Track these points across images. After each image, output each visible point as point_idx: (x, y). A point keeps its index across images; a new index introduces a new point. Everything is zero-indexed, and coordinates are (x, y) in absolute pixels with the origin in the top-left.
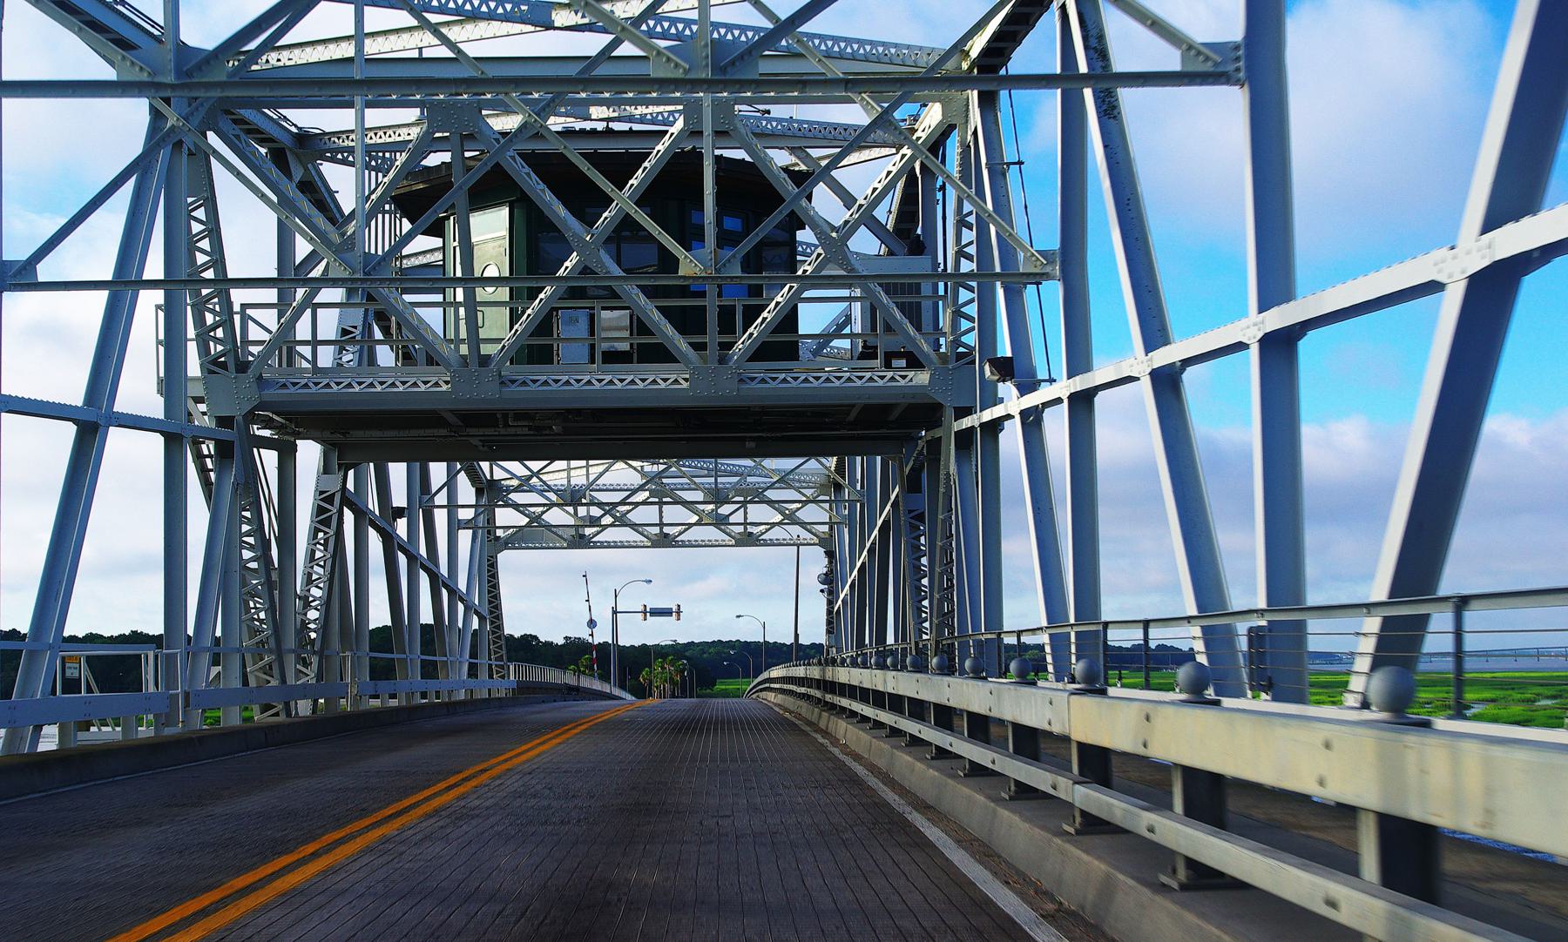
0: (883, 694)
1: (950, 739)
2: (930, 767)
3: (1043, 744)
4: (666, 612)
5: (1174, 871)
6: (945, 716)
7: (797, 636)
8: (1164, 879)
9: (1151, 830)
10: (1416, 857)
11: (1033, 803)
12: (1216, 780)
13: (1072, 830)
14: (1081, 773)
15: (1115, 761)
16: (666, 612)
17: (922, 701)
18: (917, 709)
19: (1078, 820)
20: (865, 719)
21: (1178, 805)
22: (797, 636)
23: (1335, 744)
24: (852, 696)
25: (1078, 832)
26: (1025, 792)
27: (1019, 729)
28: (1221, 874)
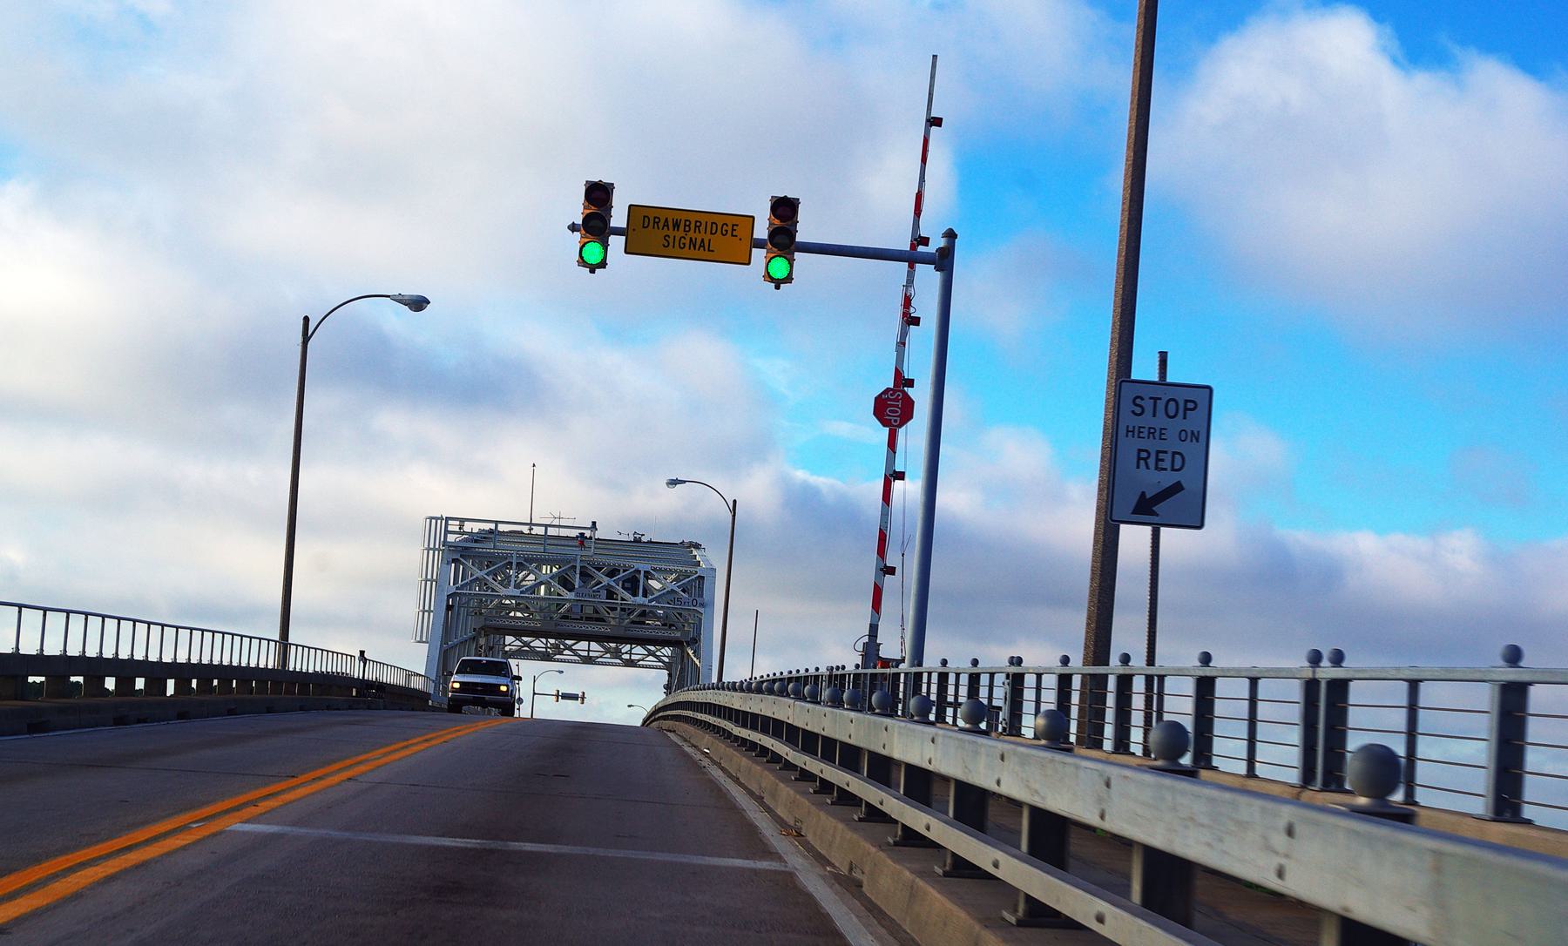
0: (815, 736)
1: (883, 795)
2: (855, 830)
3: (992, 810)
4: (573, 697)
5: (1016, 911)
6: (882, 768)
7: (284, 643)
8: (1006, 915)
9: (1100, 919)
10: (1170, 884)
11: (930, 851)
12: (983, 794)
13: (1013, 920)
14: (956, 817)
15: (1200, 883)
16: (573, 697)
17: (1300, 905)
18: (850, 757)
19: (949, 861)
20: (789, 766)
21: (1024, 846)
22: (284, 643)
23: (1298, 829)
24: (828, 757)
25: (946, 874)
26: (962, 869)
27: (912, 770)
28: (1057, 914)
